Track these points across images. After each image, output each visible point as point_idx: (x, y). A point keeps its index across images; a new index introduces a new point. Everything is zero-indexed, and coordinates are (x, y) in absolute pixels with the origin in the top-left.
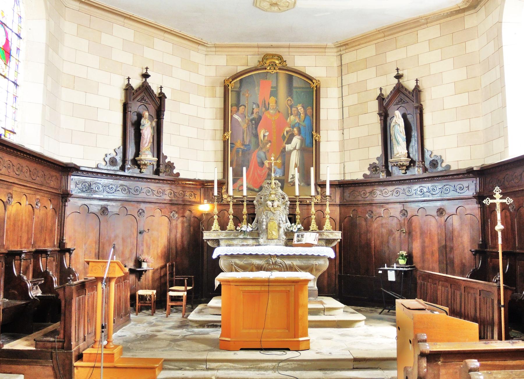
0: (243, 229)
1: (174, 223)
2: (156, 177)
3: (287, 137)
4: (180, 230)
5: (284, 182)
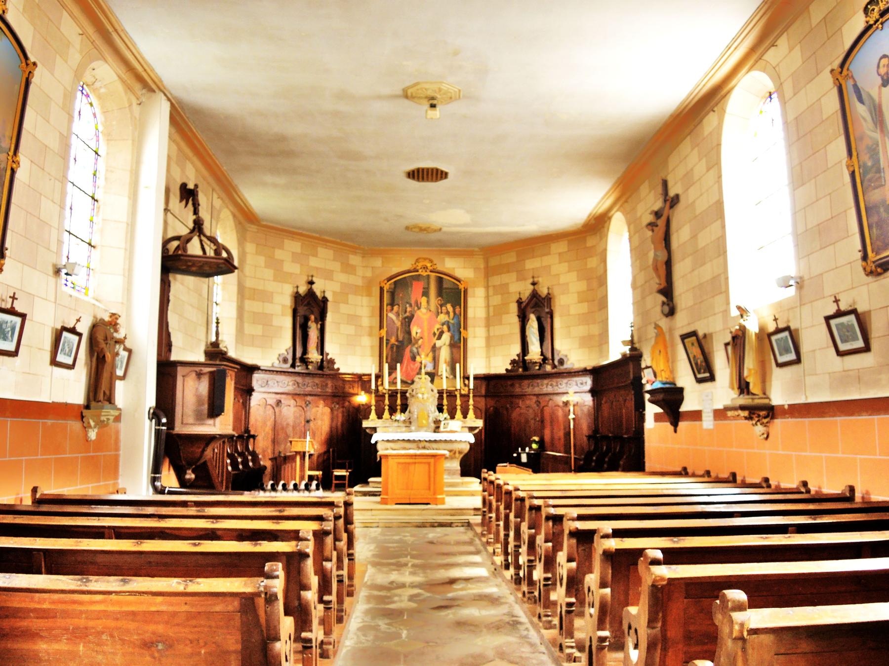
0: (397, 418)
1: (335, 413)
2: (320, 372)
3: (437, 333)
4: (340, 420)
5: (432, 376)
